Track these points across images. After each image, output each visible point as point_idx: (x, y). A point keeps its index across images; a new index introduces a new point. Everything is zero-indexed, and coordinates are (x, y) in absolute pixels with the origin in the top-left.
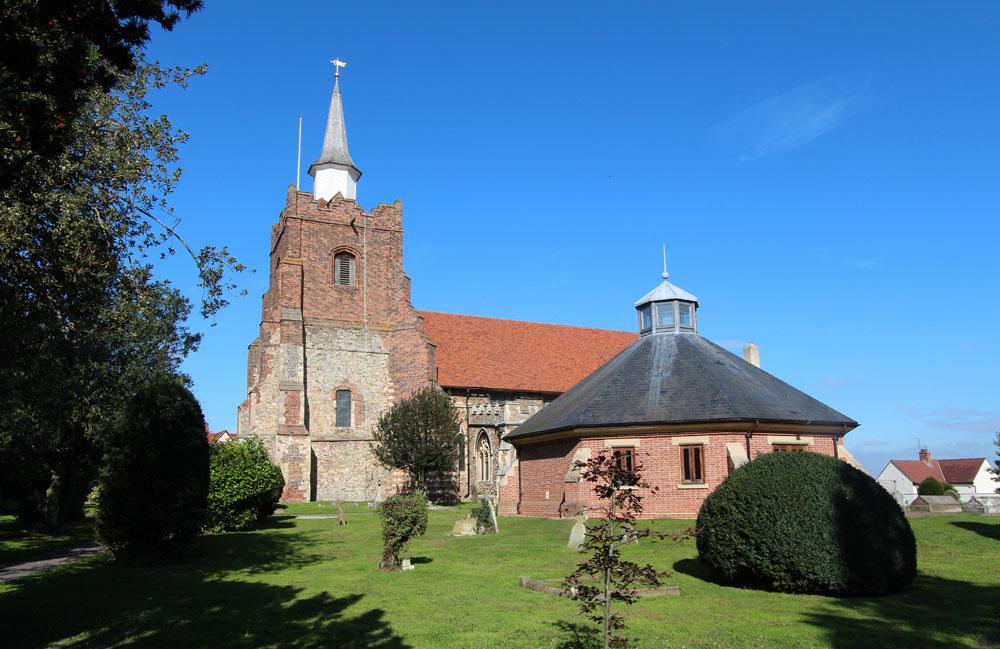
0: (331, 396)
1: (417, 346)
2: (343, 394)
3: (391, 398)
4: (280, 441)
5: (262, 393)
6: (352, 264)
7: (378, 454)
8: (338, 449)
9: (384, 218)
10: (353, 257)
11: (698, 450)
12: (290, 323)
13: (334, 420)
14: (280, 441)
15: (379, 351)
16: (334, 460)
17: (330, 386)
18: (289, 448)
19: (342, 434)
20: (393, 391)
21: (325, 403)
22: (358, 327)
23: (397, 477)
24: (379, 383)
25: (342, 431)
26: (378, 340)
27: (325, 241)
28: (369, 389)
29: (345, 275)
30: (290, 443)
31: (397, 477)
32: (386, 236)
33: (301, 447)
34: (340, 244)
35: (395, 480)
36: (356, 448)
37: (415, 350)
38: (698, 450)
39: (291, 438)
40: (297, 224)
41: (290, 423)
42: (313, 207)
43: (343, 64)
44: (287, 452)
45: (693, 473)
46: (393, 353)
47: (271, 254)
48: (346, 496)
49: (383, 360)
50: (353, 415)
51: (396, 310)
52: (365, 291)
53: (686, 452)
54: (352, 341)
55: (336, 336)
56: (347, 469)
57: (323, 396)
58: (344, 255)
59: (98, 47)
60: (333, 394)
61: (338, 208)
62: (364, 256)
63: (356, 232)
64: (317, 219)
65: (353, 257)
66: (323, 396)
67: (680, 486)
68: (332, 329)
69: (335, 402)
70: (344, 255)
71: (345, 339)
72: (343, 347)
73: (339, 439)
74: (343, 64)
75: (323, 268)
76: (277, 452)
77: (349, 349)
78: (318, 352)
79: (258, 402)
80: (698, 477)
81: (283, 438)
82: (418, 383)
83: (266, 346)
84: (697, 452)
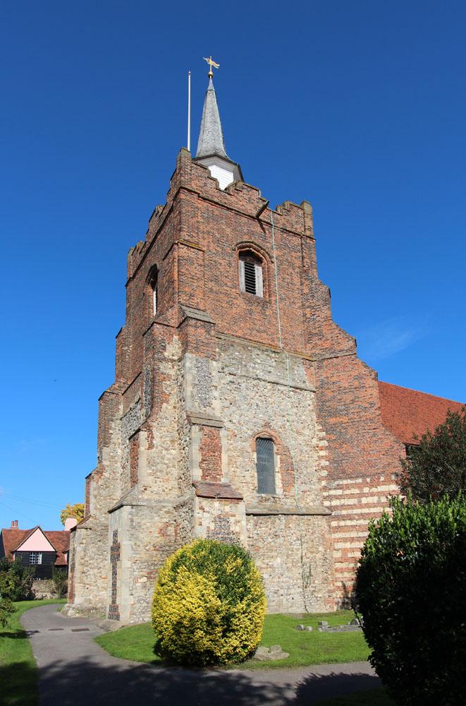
0: (249, 445)
1: (359, 377)
2: (265, 442)
3: (323, 453)
4: (201, 508)
5: (156, 434)
7: (236, 533)
12: (199, 323)
14: (201, 508)
15: (302, 386)
16: (260, 544)
17: (248, 431)
18: (215, 521)
19: (268, 504)
20: (324, 443)
21: (242, 455)
23: (342, 571)
24: (307, 432)
25: (267, 500)
26: (301, 371)
27: (228, 230)
28: (296, 440)
30: (216, 513)
31: (342, 571)
33: (232, 520)
34: (246, 238)
35: (339, 575)
36: (287, 527)
37: (356, 383)
39: (216, 504)
41: (208, 480)
43: (217, 66)
44: (212, 526)
46: (320, 391)
47: (86, 478)
48: (280, 604)
50: (278, 477)
51: (320, 335)
54: (269, 369)
55: (252, 360)
56: (279, 560)
57: (239, 444)
60: (252, 442)
61: (241, 194)
62: (274, 260)
63: (263, 229)
64: (216, 200)
66: (239, 444)
68: (245, 347)
69: (255, 455)
72: (261, 375)
73: (265, 511)
74: (217, 66)
76: (197, 527)
77: (268, 378)
78: (231, 378)
79: (151, 446)
81: (205, 503)
83: (161, 360)
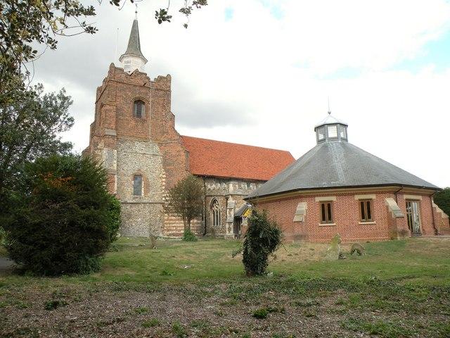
2: (137, 177)
3: (164, 180)
6: (143, 107)
8: (135, 208)
9: (161, 83)
10: (144, 103)
11: (369, 203)
13: (133, 191)
22: (146, 140)
29: (139, 114)
32: (161, 93)
38: (369, 203)
40: (115, 84)
42: (123, 76)
45: (366, 215)
49: (160, 160)
52: (150, 122)
53: (362, 204)
58: (139, 102)
59: (63, 136)
65: (144, 103)
67: (360, 223)
70: (139, 102)
71: (139, 147)
75: (128, 108)
80: (369, 217)
82: (181, 176)
84: (368, 203)
